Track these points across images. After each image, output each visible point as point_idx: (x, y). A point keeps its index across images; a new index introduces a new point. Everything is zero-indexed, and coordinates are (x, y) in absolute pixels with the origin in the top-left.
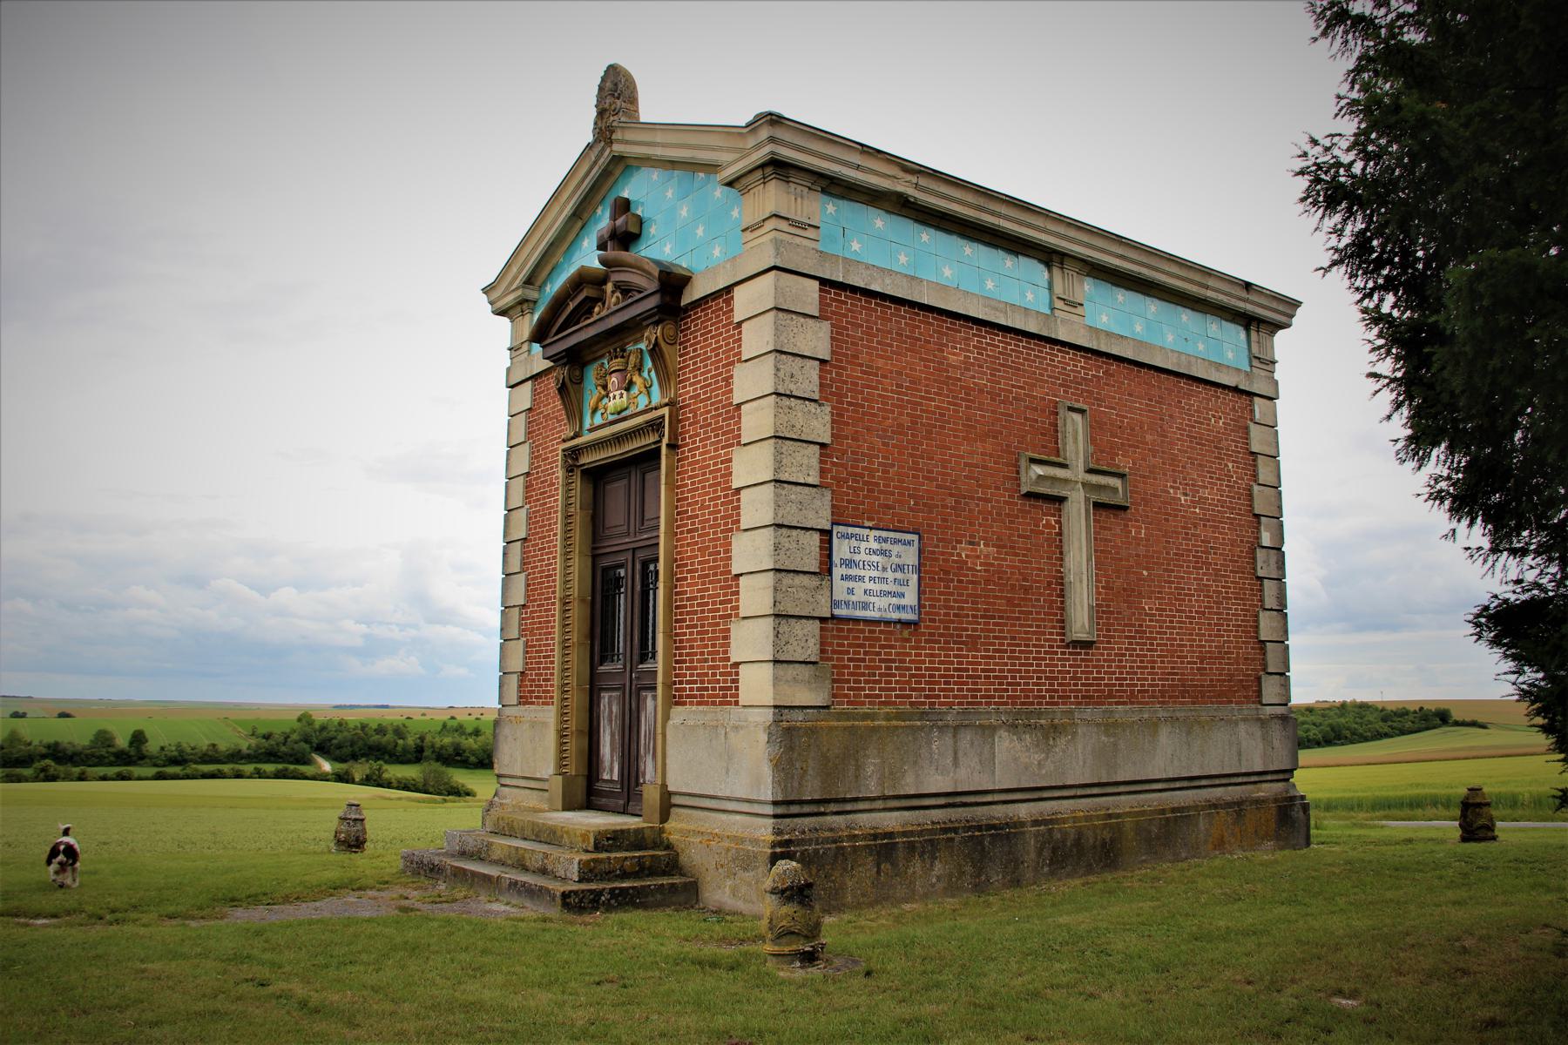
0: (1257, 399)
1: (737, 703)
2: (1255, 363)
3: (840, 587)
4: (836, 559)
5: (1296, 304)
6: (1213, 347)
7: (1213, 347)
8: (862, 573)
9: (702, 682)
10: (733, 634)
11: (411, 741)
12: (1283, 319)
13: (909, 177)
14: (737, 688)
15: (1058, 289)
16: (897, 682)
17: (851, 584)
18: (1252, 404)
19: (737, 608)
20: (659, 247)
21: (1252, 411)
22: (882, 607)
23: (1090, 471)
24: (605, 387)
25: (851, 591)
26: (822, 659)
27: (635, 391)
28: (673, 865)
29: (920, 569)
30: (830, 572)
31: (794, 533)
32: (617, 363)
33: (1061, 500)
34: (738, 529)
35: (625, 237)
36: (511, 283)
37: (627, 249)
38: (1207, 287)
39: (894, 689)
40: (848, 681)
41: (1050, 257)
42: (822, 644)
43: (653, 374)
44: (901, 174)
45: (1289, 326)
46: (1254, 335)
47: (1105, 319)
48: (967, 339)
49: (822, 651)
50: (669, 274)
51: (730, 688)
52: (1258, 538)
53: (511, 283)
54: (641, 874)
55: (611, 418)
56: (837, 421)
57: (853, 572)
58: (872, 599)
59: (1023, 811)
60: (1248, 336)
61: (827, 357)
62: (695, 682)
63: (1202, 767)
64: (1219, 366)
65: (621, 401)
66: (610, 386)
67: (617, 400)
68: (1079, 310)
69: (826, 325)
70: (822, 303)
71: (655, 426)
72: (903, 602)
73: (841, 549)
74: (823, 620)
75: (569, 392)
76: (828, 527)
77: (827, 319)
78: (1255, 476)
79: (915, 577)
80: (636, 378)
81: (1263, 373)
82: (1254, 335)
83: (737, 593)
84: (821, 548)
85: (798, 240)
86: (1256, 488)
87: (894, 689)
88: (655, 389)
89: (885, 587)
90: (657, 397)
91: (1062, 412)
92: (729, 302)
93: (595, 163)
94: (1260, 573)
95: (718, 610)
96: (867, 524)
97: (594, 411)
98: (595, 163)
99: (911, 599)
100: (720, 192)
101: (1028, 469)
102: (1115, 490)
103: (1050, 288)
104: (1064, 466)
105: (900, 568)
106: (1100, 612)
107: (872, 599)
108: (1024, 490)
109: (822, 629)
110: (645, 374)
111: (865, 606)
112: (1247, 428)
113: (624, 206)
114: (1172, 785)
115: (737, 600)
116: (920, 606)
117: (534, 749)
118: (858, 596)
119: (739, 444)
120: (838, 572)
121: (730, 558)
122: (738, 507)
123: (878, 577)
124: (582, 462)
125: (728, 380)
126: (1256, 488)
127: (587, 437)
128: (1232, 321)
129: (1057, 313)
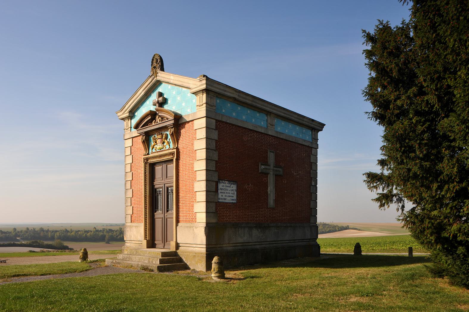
0: (313, 149)
1: (196, 222)
2: (313, 140)
3: (220, 195)
4: (219, 188)
5: (325, 125)
6: (304, 136)
7: (304, 136)
8: (225, 191)
9: (186, 217)
10: (195, 206)
11: (50, 235)
12: (320, 129)
13: (237, 93)
14: (196, 218)
15: (269, 121)
16: (232, 217)
17: (222, 194)
18: (312, 150)
19: (196, 199)
20: (171, 107)
21: (312, 152)
22: (229, 200)
23: (274, 167)
24: (156, 142)
25: (222, 196)
26: (216, 212)
27: (165, 144)
28: (181, 260)
29: (237, 191)
30: (218, 191)
31: (210, 182)
32: (159, 136)
33: (268, 174)
34: (196, 181)
35: (162, 103)
36: (125, 111)
37: (161, 107)
38: (304, 121)
39: (231, 219)
40: (221, 217)
41: (268, 113)
42: (216, 208)
43: (171, 140)
44: (235, 93)
45: (322, 130)
46: (313, 132)
47: (279, 129)
48: (248, 134)
49: (216, 210)
50: (176, 115)
51: (194, 218)
52: (311, 183)
53: (125, 111)
54: (173, 262)
55: (158, 150)
56: (219, 156)
57: (223, 191)
58: (227, 198)
59: (258, 247)
60: (312, 133)
61: (217, 140)
62: (184, 217)
63: (189, 264)
64: (305, 140)
65: (161, 147)
66: (157, 142)
67: (159, 146)
68: (274, 127)
69: (217, 131)
70: (216, 126)
71: (172, 154)
72: (233, 198)
73: (220, 186)
74: (216, 203)
75: (147, 142)
76: (217, 180)
77: (217, 130)
78: (311, 168)
79: (236, 192)
80: (165, 141)
81: (315, 142)
82: (313, 132)
83: (196, 196)
84: (216, 186)
85: (211, 109)
86: (311, 171)
87: (231, 219)
88: (171, 144)
89: (229, 195)
90: (172, 146)
91: (269, 152)
92: (193, 124)
93: (151, 81)
94: (311, 192)
95: (190, 200)
96: (225, 180)
97: (153, 148)
98: (151, 81)
99: (235, 198)
100: (189, 95)
101: (261, 166)
102: (280, 171)
103: (267, 121)
104: (269, 166)
105: (233, 190)
106: (276, 201)
107: (227, 198)
108: (260, 171)
109: (216, 205)
110: (168, 140)
111: (225, 199)
112: (310, 156)
113: (161, 94)
114: (290, 242)
115: (196, 198)
116: (237, 199)
117: (136, 234)
118: (224, 197)
119: (196, 160)
120: (219, 191)
121: (194, 188)
122: (196, 175)
123: (228, 193)
124: (149, 161)
125: (192, 144)
126: (311, 171)
127: (151, 155)
128: (309, 129)
129: (269, 127)
